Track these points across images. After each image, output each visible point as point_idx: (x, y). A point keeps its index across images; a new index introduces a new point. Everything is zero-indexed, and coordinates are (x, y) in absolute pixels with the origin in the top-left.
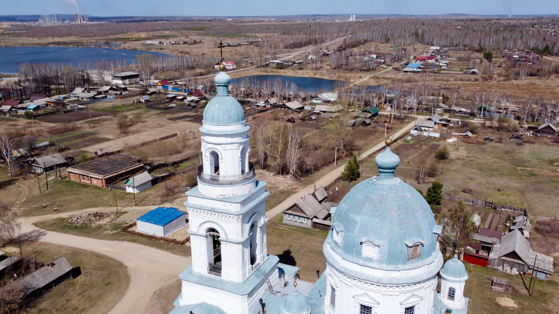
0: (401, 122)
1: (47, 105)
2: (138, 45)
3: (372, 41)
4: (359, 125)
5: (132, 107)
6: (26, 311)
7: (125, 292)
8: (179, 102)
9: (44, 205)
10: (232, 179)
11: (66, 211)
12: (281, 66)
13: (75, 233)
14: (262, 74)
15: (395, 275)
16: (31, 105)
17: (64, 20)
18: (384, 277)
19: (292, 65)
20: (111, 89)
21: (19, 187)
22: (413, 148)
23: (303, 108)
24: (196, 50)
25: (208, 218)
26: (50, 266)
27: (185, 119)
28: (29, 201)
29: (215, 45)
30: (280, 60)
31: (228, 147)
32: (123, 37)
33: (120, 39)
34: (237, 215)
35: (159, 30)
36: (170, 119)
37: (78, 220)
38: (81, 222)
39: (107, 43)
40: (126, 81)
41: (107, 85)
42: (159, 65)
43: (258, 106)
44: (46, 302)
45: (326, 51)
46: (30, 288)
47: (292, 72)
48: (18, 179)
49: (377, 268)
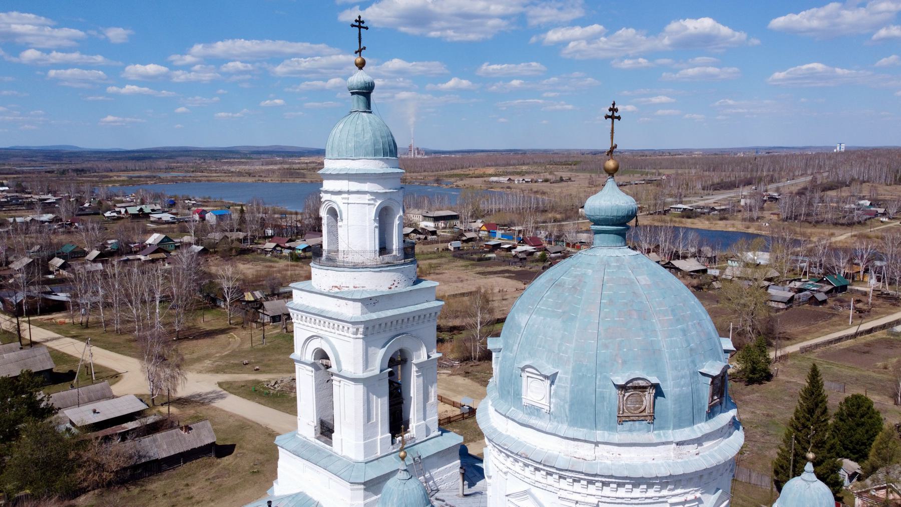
0: (894, 305)
2: (478, 183)
3: (868, 181)
4: (804, 303)
5: (433, 256)
6: (127, 489)
8: (503, 253)
9: (246, 361)
10: (358, 259)
11: (269, 372)
12: (690, 213)
13: (263, 401)
15: (585, 451)
18: (562, 455)
19: (709, 213)
20: (415, 231)
21: (232, 337)
23: (705, 271)
24: (558, 190)
25: (316, 331)
26: (184, 430)
27: (502, 275)
28: (233, 355)
29: (589, 183)
30: (690, 205)
31: (353, 198)
32: (462, 173)
34: (353, 323)
35: (514, 165)
36: (478, 273)
37: (276, 386)
38: (279, 388)
39: (438, 181)
40: (440, 224)
41: (410, 226)
42: (494, 207)
44: (160, 482)
45: (776, 194)
46: (145, 457)
47: (707, 222)
48: (236, 328)
49: (547, 430)
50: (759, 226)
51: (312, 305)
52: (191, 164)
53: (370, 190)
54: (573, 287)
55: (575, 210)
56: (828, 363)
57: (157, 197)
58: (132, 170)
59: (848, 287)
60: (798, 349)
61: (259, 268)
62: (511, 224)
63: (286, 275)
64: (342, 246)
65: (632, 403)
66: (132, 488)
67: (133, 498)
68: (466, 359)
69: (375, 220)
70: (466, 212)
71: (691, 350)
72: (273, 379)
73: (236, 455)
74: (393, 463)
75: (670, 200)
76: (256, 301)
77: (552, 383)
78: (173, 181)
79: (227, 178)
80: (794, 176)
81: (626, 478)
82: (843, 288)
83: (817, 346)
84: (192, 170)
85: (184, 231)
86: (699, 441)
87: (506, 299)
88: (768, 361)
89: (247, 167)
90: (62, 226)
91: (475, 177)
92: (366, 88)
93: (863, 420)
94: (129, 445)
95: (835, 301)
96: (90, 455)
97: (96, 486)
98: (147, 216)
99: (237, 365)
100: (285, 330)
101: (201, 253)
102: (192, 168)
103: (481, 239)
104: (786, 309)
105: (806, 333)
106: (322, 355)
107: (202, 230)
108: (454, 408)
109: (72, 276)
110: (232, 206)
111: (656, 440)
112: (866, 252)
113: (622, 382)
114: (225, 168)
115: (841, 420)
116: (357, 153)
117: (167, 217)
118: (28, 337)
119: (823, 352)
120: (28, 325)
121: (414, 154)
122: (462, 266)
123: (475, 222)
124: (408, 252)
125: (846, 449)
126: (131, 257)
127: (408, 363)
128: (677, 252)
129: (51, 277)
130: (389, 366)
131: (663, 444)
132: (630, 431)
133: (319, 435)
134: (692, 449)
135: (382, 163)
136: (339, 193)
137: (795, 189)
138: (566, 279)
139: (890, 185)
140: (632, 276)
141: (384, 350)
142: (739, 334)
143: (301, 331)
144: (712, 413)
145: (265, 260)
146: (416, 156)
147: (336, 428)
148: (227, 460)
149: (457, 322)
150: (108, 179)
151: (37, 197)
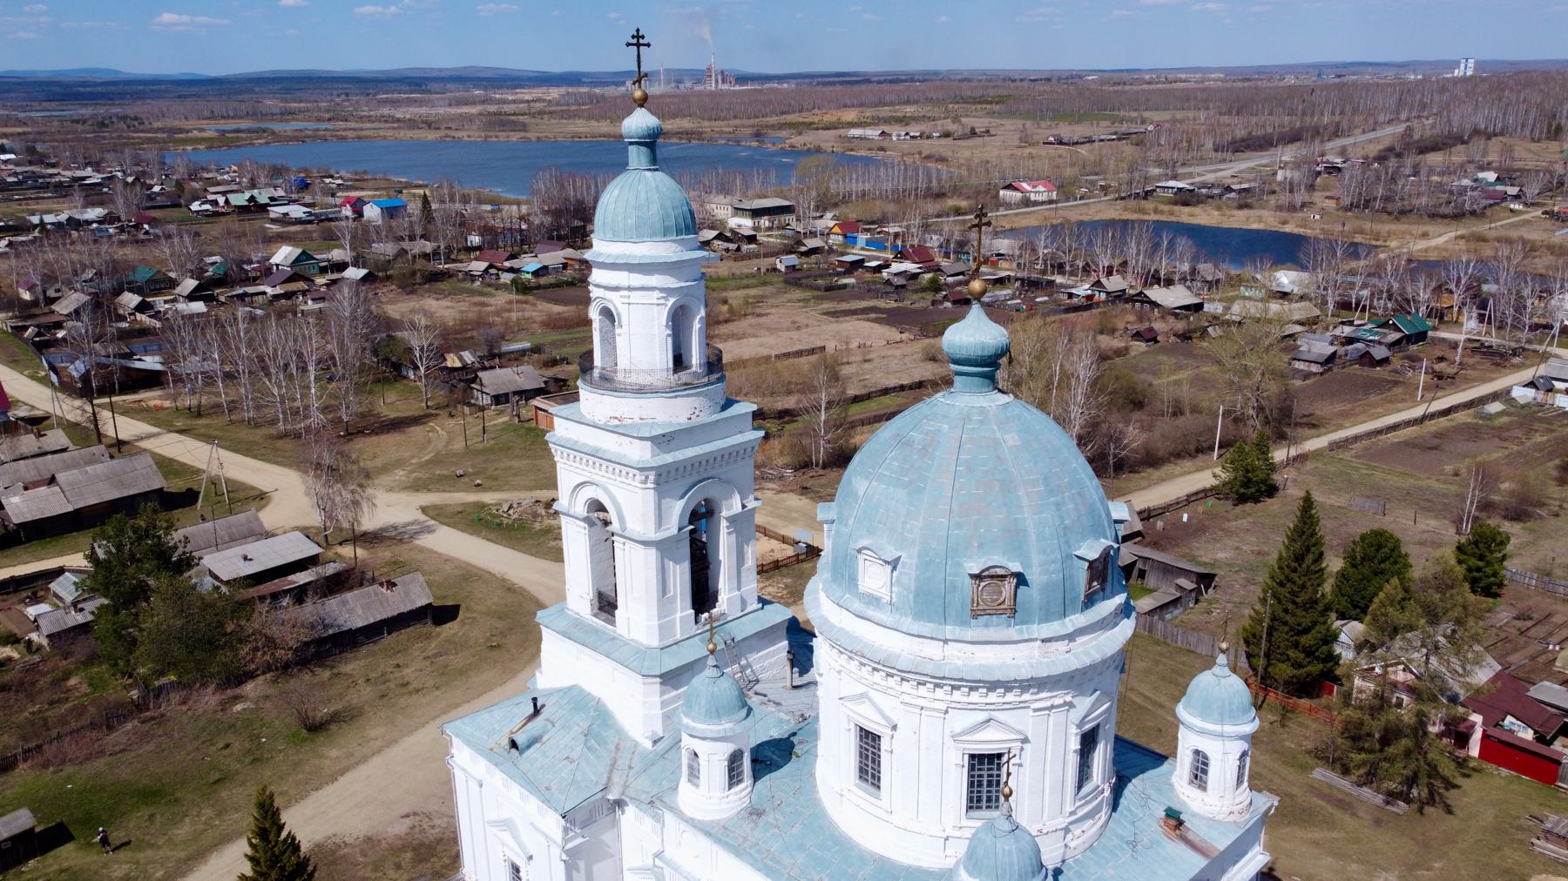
0: (1497, 365)
1: (565, 266)
2: (827, 139)
3: (1502, 134)
4: (1353, 362)
5: (751, 281)
7: (519, 672)
8: (868, 276)
10: (644, 380)
11: (498, 489)
13: (492, 536)
14: (1127, 216)
15: (932, 650)
16: (529, 264)
17: (679, 82)
19: (1221, 196)
20: (720, 237)
21: (433, 430)
22: (1498, 437)
24: (967, 154)
28: (437, 461)
29: (1021, 140)
30: (1190, 181)
31: (636, 296)
32: (801, 120)
33: (791, 125)
34: (642, 470)
35: (892, 104)
36: (824, 314)
37: (511, 512)
38: (516, 516)
39: (758, 135)
41: (712, 228)
42: (856, 187)
43: (1071, 296)
47: (1216, 213)
48: (437, 415)
49: (888, 624)
50: (1304, 220)
51: (583, 440)
52: (324, 104)
53: (658, 285)
54: (924, 448)
55: (993, 192)
56: (1369, 467)
57: (277, 172)
58: (223, 117)
59: (1430, 333)
60: (1326, 444)
61: (463, 306)
62: (882, 221)
63: (509, 319)
64: (623, 363)
65: (989, 594)
66: (318, 670)
67: (323, 685)
68: (804, 465)
69: (667, 326)
70: (806, 203)
71: (1065, 528)
72: (507, 501)
73: (462, 621)
74: (695, 650)
75: (1155, 171)
76: (465, 368)
77: (894, 568)
78: (296, 139)
79: (390, 133)
80: (1376, 123)
81: (979, 681)
82: (1421, 336)
83: (1356, 438)
84: (328, 116)
85: (331, 238)
86: (1071, 637)
87: (869, 360)
88: (1273, 468)
89: (423, 110)
90: (122, 230)
91: (824, 129)
92: (649, 136)
93: (1383, 566)
94: (310, 610)
95: (1403, 358)
96: (256, 626)
97: (268, 668)
98: (263, 208)
99: (445, 477)
100: (516, 419)
101: (365, 279)
102: (328, 111)
103: (831, 251)
104: (1322, 374)
105: (1345, 415)
106: (598, 507)
107: (363, 236)
108: (785, 546)
109: (158, 325)
110: (405, 188)
111: (1017, 637)
112: (1466, 273)
113: (977, 571)
114: (385, 111)
115: (1354, 566)
116: (639, 233)
117: (297, 211)
118: (111, 433)
119: (1366, 449)
120: (110, 414)
121: (717, 81)
122: (799, 301)
123: (821, 217)
124: (714, 365)
125: (1355, 607)
126: (251, 290)
127: (715, 516)
128: (1157, 271)
129: (124, 325)
130: (691, 523)
131: (1026, 641)
132: (986, 626)
133: (596, 610)
134: (1062, 646)
135: (674, 245)
136: (617, 289)
137: (1373, 150)
138: (917, 436)
139: (1539, 140)
140: (998, 435)
141: (684, 501)
142: (1236, 420)
143: (568, 474)
144: (1090, 601)
145: (472, 292)
146: (720, 86)
147: (620, 603)
148: (449, 629)
149: (790, 402)
150: (183, 136)
151: (69, 173)
